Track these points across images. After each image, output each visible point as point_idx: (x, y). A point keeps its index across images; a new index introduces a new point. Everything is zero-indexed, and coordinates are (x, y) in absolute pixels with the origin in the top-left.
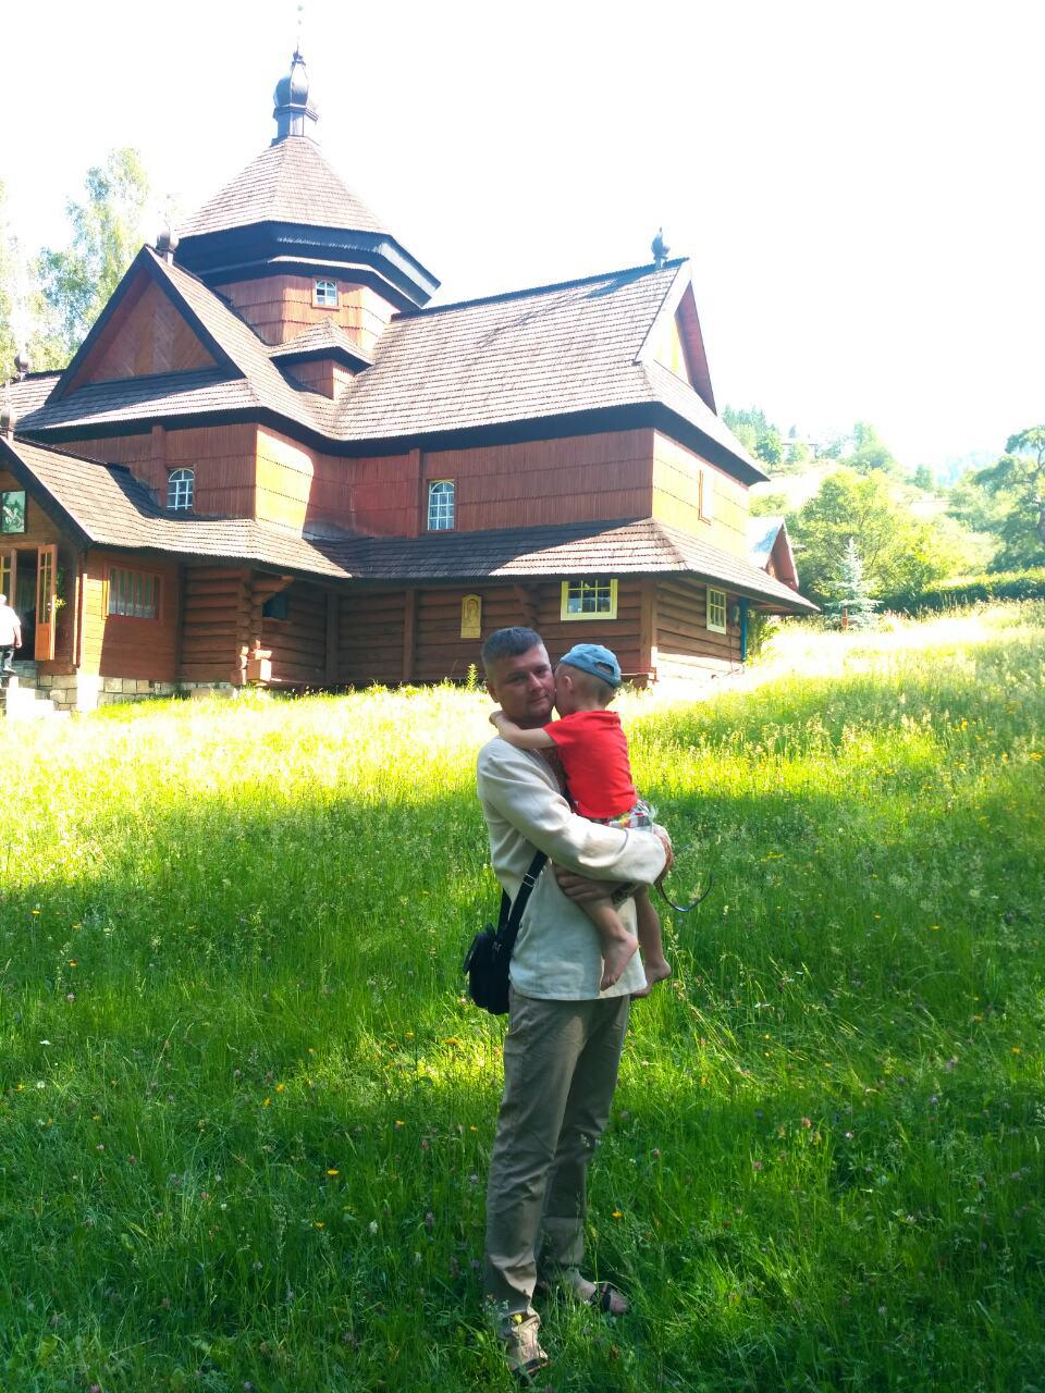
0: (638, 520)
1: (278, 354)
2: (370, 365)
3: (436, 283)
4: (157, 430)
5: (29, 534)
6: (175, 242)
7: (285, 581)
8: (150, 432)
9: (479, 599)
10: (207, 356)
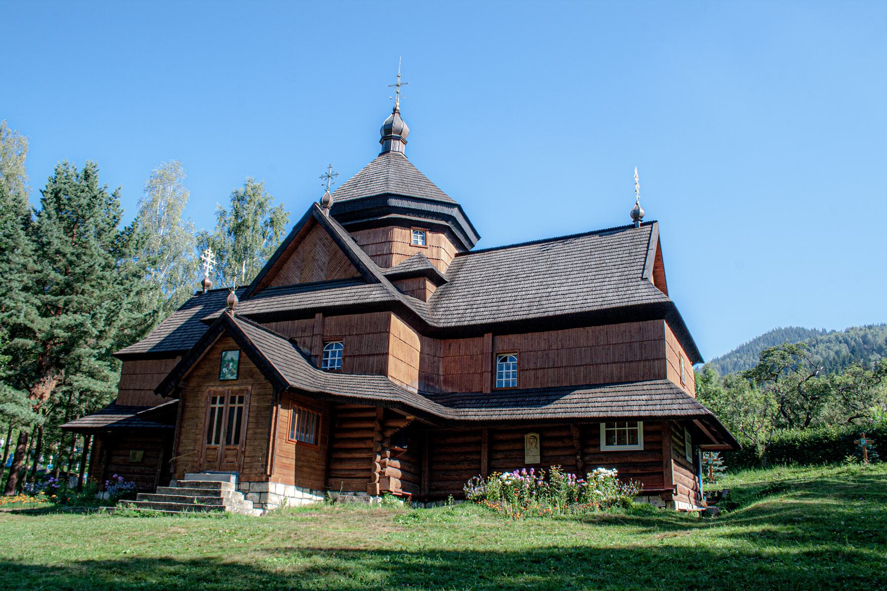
0: (636, 382)
1: (390, 273)
2: (447, 282)
3: (478, 237)
4: (319, 316)
5: (239, 380)
6: (332, 201)
7: (408, 420)
8: (314, 317)
9: (537, 436)
10: (353, 269)
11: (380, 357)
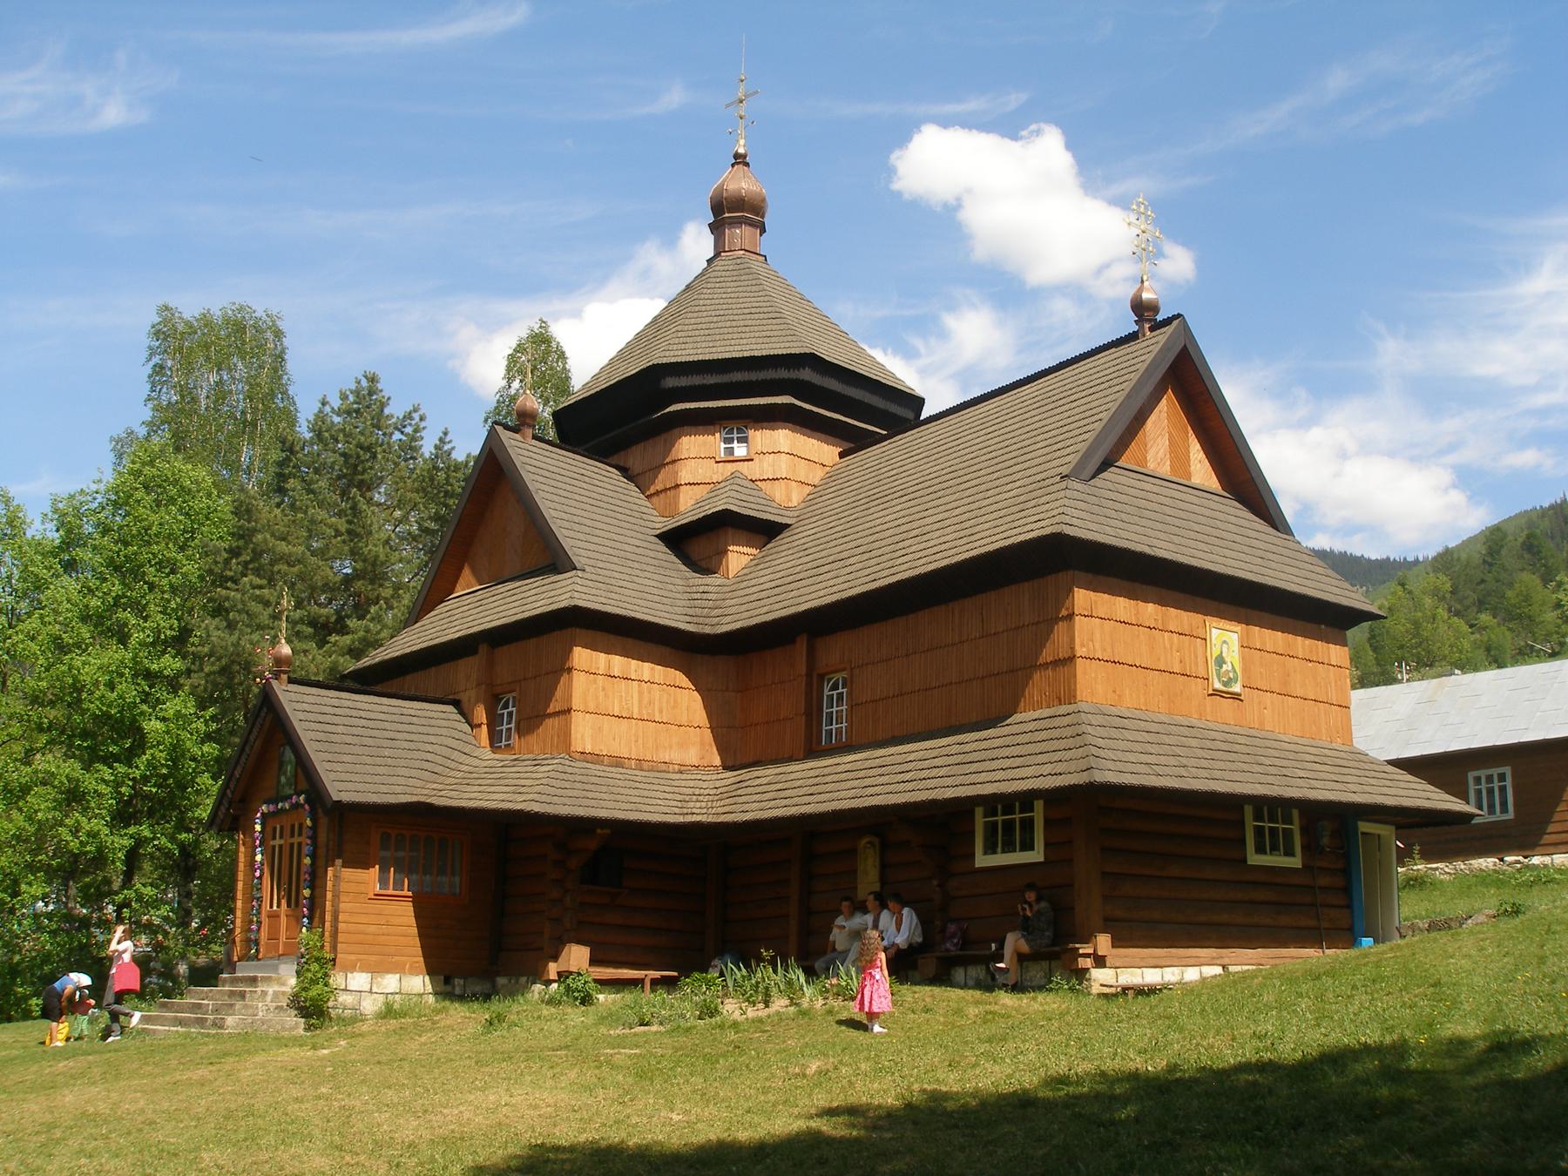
11: (562, 717)
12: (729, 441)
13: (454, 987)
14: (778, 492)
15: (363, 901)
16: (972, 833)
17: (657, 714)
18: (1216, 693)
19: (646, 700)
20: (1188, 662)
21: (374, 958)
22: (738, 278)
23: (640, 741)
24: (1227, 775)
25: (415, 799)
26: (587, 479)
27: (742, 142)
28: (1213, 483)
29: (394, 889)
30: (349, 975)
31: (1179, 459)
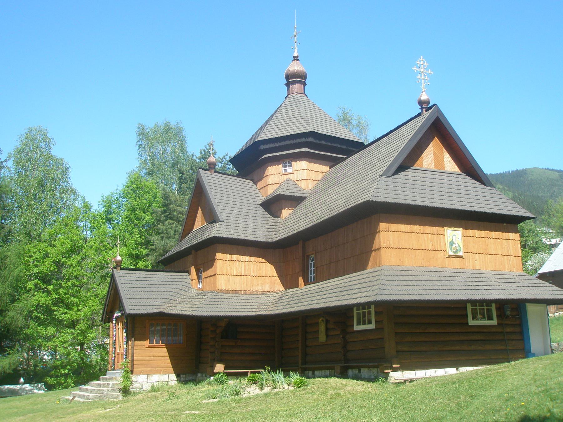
12: (285, 167)
13: (181, 378)
14: (303, 185)
15: (143, 348)
16: (353, 316)
17: (252, 273)
18: (450, 256)
19: (247, 268)
20: (436, 245)
21: (148, 369)
22: (293, 104)
23: (245, 284)
24: (445, 292)
25: (159, 311)
26: (234, 186)
27: (296, 51)
28: (456, 169)
29: (156, 343)
30: (138, 376)
31: (439, 161)
